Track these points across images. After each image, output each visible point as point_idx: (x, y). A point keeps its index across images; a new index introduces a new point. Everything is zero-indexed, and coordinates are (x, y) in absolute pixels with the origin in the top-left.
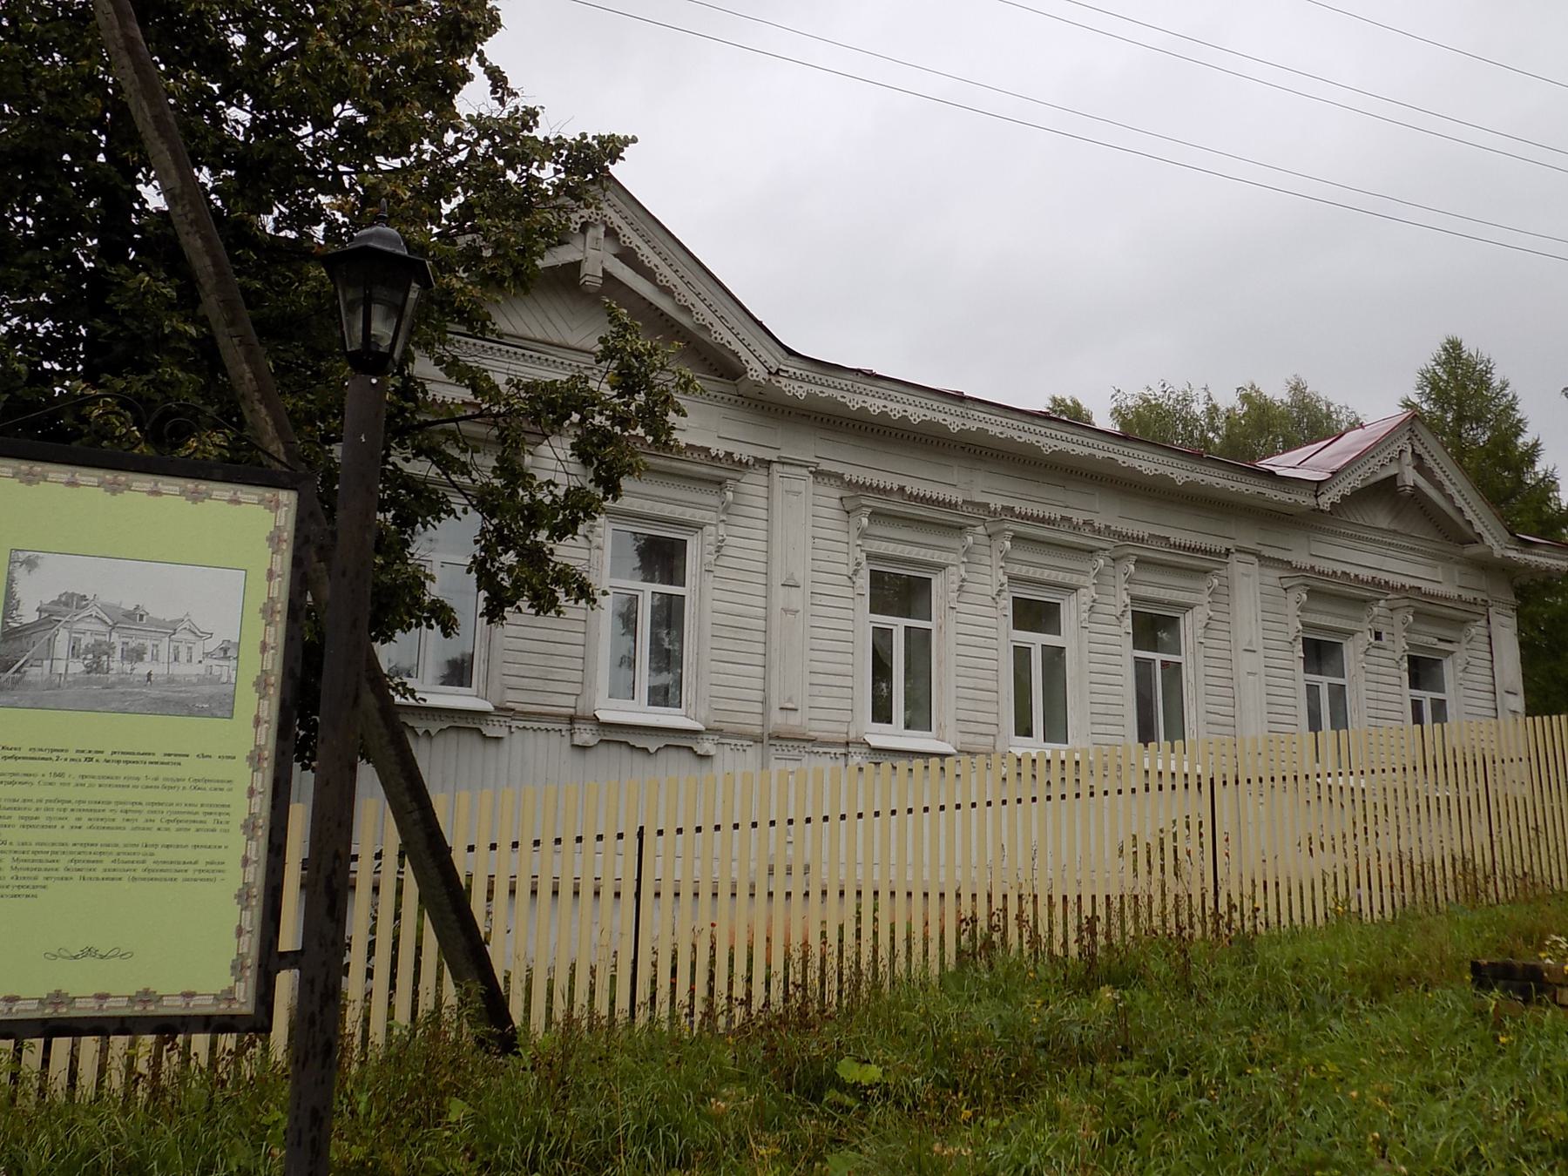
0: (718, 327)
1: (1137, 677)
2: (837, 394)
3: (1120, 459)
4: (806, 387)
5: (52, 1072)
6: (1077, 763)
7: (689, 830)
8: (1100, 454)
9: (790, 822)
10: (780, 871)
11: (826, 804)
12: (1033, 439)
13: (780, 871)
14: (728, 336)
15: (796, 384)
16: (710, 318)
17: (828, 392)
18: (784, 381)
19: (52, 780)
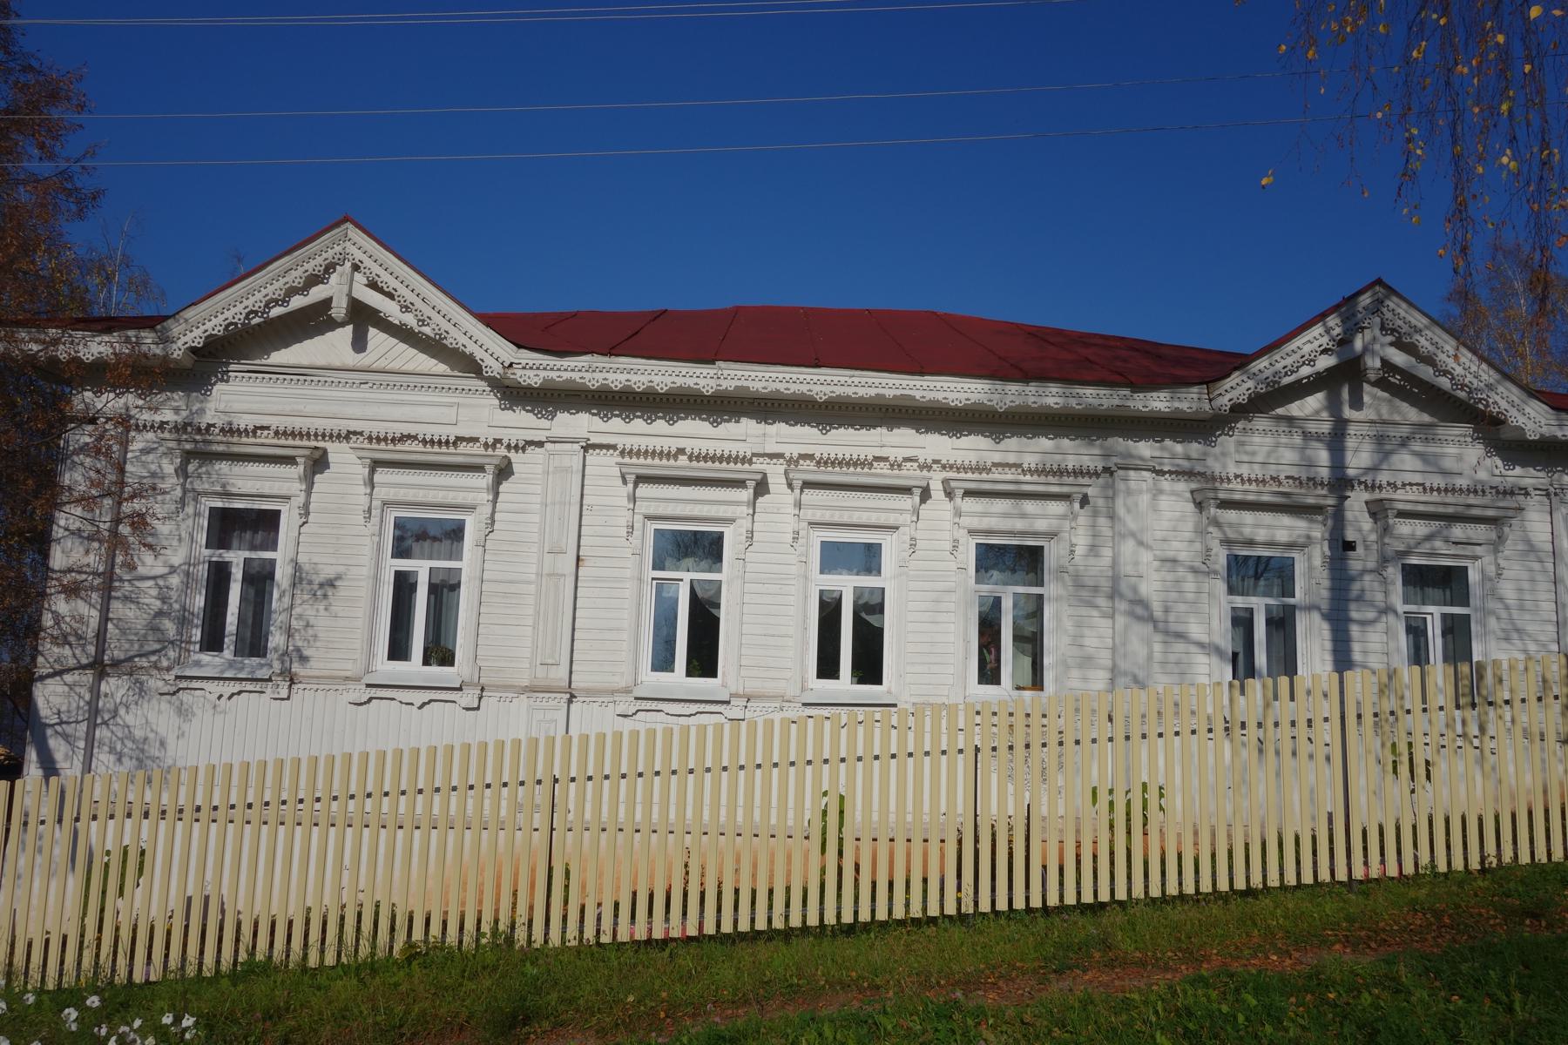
0: (454, 332)
1: (817, 365)
2: (576, 376)
3: (918, 395)
4: (543, 374)
5: (16, 960)
6: (1144, 785)
7: (1086, 742)
8: (889, 393)
9: (1111, 739)
10: (1169, 711)
11: (251, 792)
12: (804, 388)
13: (1169, 711)
14: (463, 340)
15: (531, 373)
16: (445, 325)
17: (566, 375)
18: (519, 373)
19: (1389, 745)
